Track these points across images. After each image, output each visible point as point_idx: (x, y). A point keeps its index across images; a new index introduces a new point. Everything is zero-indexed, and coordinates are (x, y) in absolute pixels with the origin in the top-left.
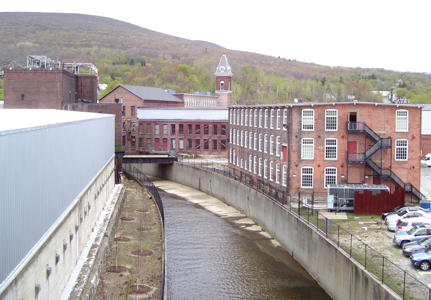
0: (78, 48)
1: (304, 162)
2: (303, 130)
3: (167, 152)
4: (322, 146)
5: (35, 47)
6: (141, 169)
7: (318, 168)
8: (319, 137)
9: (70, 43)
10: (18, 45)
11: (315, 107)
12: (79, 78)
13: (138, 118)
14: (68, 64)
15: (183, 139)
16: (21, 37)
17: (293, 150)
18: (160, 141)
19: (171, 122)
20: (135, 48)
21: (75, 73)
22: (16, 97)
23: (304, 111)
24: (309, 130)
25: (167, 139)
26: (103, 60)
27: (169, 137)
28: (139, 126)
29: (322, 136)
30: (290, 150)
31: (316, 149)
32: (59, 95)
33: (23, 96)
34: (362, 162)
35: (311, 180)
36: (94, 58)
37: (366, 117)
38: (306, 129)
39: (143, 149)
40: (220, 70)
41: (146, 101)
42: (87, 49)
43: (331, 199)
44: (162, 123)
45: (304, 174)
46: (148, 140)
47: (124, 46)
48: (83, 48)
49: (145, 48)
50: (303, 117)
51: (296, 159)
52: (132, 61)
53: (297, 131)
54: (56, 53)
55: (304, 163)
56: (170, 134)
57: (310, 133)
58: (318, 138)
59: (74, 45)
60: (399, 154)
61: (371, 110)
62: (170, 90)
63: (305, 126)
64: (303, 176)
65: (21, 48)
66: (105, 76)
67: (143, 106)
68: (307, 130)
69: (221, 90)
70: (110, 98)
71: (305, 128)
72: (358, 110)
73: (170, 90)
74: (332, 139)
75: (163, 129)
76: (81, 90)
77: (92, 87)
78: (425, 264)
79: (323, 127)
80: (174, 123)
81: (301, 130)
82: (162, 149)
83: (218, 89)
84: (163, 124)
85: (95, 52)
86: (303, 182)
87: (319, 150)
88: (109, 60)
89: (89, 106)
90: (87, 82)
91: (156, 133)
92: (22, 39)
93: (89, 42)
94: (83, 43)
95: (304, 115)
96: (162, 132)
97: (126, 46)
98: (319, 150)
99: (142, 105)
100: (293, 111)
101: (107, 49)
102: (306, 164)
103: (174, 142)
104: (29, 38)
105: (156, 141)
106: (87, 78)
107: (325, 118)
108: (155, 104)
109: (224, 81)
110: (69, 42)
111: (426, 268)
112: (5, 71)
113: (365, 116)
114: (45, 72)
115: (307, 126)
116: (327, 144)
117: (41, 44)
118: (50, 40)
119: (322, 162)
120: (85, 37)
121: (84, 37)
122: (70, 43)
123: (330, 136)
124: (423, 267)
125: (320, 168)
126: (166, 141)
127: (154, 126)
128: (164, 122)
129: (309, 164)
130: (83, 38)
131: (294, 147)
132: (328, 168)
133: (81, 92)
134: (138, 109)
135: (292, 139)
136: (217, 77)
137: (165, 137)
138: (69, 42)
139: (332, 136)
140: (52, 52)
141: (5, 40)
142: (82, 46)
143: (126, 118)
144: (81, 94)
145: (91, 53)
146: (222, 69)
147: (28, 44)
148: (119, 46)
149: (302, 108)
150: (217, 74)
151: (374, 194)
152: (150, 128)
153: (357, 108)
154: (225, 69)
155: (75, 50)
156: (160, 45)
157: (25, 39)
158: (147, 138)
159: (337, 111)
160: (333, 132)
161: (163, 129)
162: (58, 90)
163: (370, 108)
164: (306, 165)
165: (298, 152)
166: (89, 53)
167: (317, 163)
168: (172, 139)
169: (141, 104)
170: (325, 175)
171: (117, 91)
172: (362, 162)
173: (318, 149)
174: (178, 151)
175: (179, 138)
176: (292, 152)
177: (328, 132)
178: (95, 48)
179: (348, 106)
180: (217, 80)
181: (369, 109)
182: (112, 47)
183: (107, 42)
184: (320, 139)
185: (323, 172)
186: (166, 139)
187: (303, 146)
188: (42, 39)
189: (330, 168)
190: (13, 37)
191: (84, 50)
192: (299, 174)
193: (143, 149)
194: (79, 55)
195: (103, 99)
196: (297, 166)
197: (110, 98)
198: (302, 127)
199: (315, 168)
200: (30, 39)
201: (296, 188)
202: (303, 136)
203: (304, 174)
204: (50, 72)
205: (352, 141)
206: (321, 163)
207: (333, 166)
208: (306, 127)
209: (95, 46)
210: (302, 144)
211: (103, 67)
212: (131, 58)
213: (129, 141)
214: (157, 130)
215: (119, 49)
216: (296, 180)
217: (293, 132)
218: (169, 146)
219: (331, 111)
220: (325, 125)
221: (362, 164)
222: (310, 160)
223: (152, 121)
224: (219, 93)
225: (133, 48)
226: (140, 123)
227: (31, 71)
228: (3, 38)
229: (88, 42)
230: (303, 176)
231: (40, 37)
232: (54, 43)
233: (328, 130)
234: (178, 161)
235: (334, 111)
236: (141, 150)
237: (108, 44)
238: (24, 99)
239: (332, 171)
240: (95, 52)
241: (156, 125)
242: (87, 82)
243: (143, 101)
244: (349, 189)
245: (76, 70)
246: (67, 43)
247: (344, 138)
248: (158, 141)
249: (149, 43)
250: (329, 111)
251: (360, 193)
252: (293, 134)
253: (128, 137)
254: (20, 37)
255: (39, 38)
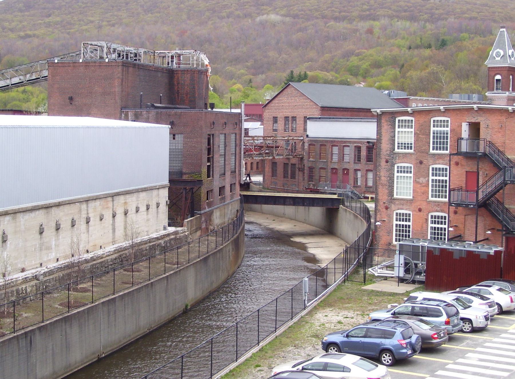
0: (355, 23)
1: (397, 202)
2: (396, 150)
3: (345, 190)
4: (426, 178)
5: (284, 23)
6: (308, 216)
7: (419, 213)
8: (421, 163)
9: (343, 14)
10: (258, 19)
11: (414, 113)
12: (176, 72)
13: (307, 136)
14: (159, 52)
15: (372, 171)
16: (265, 7)
17: (381, 182)
18: (338, 172)
19: (355, 142)
20: (453, 20)
21: (170, 65)
22: (63, 101)
23: (399, 120)
24: (407, 151)
25: (348, 169)
26: (392, 41)
27: (352, 167)
28: (309, 148)
29: (425, 162)
30: (378, 182)
31: (415, 182)
32: (117, 98)
33: (71, 99)
34: (472, 206)
35: (409, 232)
36: (379, 38)
37: (495, 130)
38: (402, 149)
39: (314, 185)
40: (494, 55)
41: (324, 109)
42: (367, 24)
43: (399, 260)
44: (342, 144)
45: (398, 223)
46: (322, 170)
47: (434, 17)
48: (362, 21)
49: (471, 19)
50: (397, 129)
51: (387, 198)
52: (443, 42)
53: (388, 152)
54: (316, 32)
55: (398, 204)
56: (353, 162)
57: (408, 155)
58: (419, 165)
59: (348, 17)
60: (442, 187)
61: (503, 118)
62: (393, 92)
63: (400, 145)
64: (397, 225)
65: (263, 24)
66: (392, 69)
67: (320, 117)
68: (403, 151)
69: (495, 91)
70: (278, 103)
71: (400, 147)
72: (483, 119)
73: (393, 92)
74: (441, 166)
75: (344, 154)
76: (178, 91)
77: (193, 86)
78: (389, 356)
79: (427, 146)
80: (360, 145)
81: (394, 150)
82: (342, 186)
83: (491, 89)
84: (344, 146)
85: (380, 29)
86: (396, 235)
87: (421, 184)
88: (402, 42)
89: (157, 113)
90: (186, 78)
91: (334, 160)
92: (265, 9)
93: (374, 11)
94: (364, 13)
95: (399, 127)
96: (342, 159)
97: (437, 16)
98: (421, 184)
99: (318, 115)
100: (383, 121)
101: (404, 23)
102: (401, 207)
103: (359, 174)
104: (276, 9)
105: (332, 173)
106: (185, 72)
107: (430, 132)
108: (346, 113)
109: (27, 74)
110: (340, 12)
111: (386, 361)
112: (49, 65)
113: (493, 128)
114: (99, 64)
115: (406, 145)
116: (433, 175)
117: (295, 16)
118: (309, 10)
119: (425, 203)
120: (368, 3)
121: (366, 3)
122: (343, 14)
123: (437, 162)
124: (384, 357)
125: (421, 213)
126: (348, 174)
127: (330, 149)
128: (345, 142)
129: (404, 207)
130: (365, 5)
131: (383, 178)
132: (434, 214)
133: (178, 93)
134: (308, 120)
135: (380, 165)
136: (489, 68)
137: (346, 166)
138: (340, 12)
139: (441, 161)
140: (310, 31)
141: (238, 12)
142: (362, 18)
143: (298, 135)
144: (178, 96)
145: (374, 31)
146: (498, 55)
147: (273, 17)
148: (426, 16)
149: (396, 116)
150: (489, 63)
151: (456, 256)
152: (324, 151)
153: (480, 116)
154: (502, 53)
155: (349, 26)
156: (499, 12)
157: (270, 9)
158: (321, 168)
159: (449, 119)
160: (442, 155)
161: (344, 154)
162: (117, 90)
163: (501, 116)
164: (400, 207)
165: (390, 186)
166: (370, 31)
167: (417, 205)
168: (356, 170)
169: (317, 113)
170: (430, 225)
171: (287, 93)
172: (472, 206)
173: (418, 183)
174: (364, 189)
175: (366, 169)
176: (380, 187)
177: (434, 155)
178: (384, 21)
179: (466, 113)
180: (488, 73)
181: (500, 118)
182: (413, 19)
183: (405, 11)
184: (423, 166)
185: (427, 220)
186: (348, 170)
187: (397, 177)
188: (297, 10)
189: (437, 214)
190: (252, 8)
191: (363, 26)
192: (391, 221)
193: (314, 185)
194: (354, 34)
195: (269, 105)
196: (387, 208)
197: (278, 103)
198: (396, 145)
199: (415, 213)
200: (277, 10)
201: (386, 244)
202: (397, 160)
203: (398, 223)
204: (105, 64)
205: (471, 170)
206: (424, 206)
207: (442, 211)
208: (401, 146)
209: (383, 18)
210: (396, 174)
211: (389, 53)
212: (441, 38)
213: (301, 172)
214: (346, 156)
215: (423, 22)
216: (386, 231)
217: (382, 153)
218: (351, 181)
219: (441, 121)
220: (430, 143)
221: (472, 209)
222: (407, 200)
223: (327, 141)
224: (492, 96)
225: (449, 20)
226: (310, 143)
227: (81, 65)
228: (236, 10)
229: (372, 11)
230: (397, 225)
231: (293, 6)
232: (316, 14)
233: (435, 152)
234: (345, 204)
235: (444, 121)
236: (311, 186)
237: (407, 14)
238: (73, 103)
239: (440, 220)
240: (380, 29)
241: (334, 148)
242: (186, 78)
243: (319, 108)
244: (428, 247)
245: (171, 61)
246: (337, 14)
247: (459, 166)
248: (336, 173)
249: (478, 11)
250: (438, 121)
251: (481, 257)
252: (383, 157)
253: (300, 166)
254: (262, 7)
255: (292, 7)
